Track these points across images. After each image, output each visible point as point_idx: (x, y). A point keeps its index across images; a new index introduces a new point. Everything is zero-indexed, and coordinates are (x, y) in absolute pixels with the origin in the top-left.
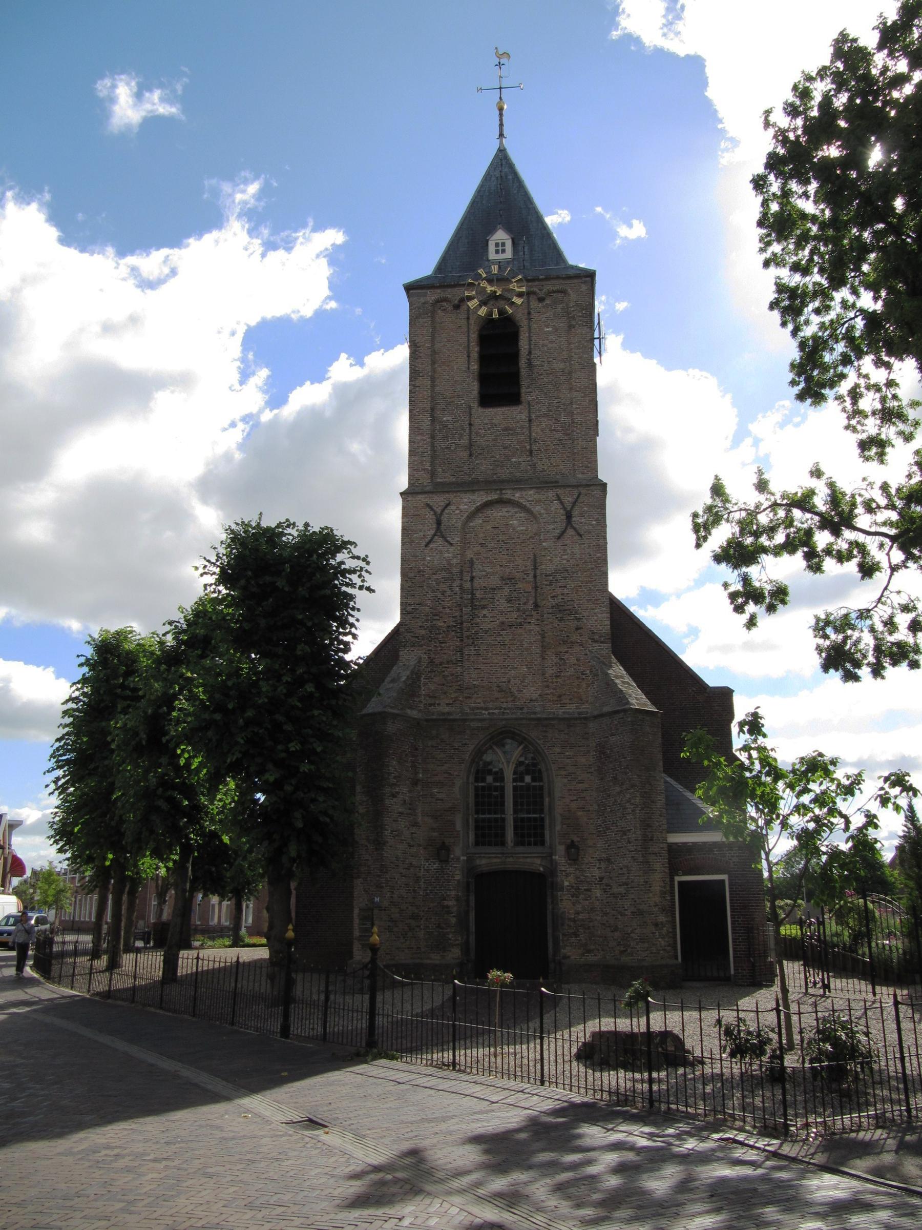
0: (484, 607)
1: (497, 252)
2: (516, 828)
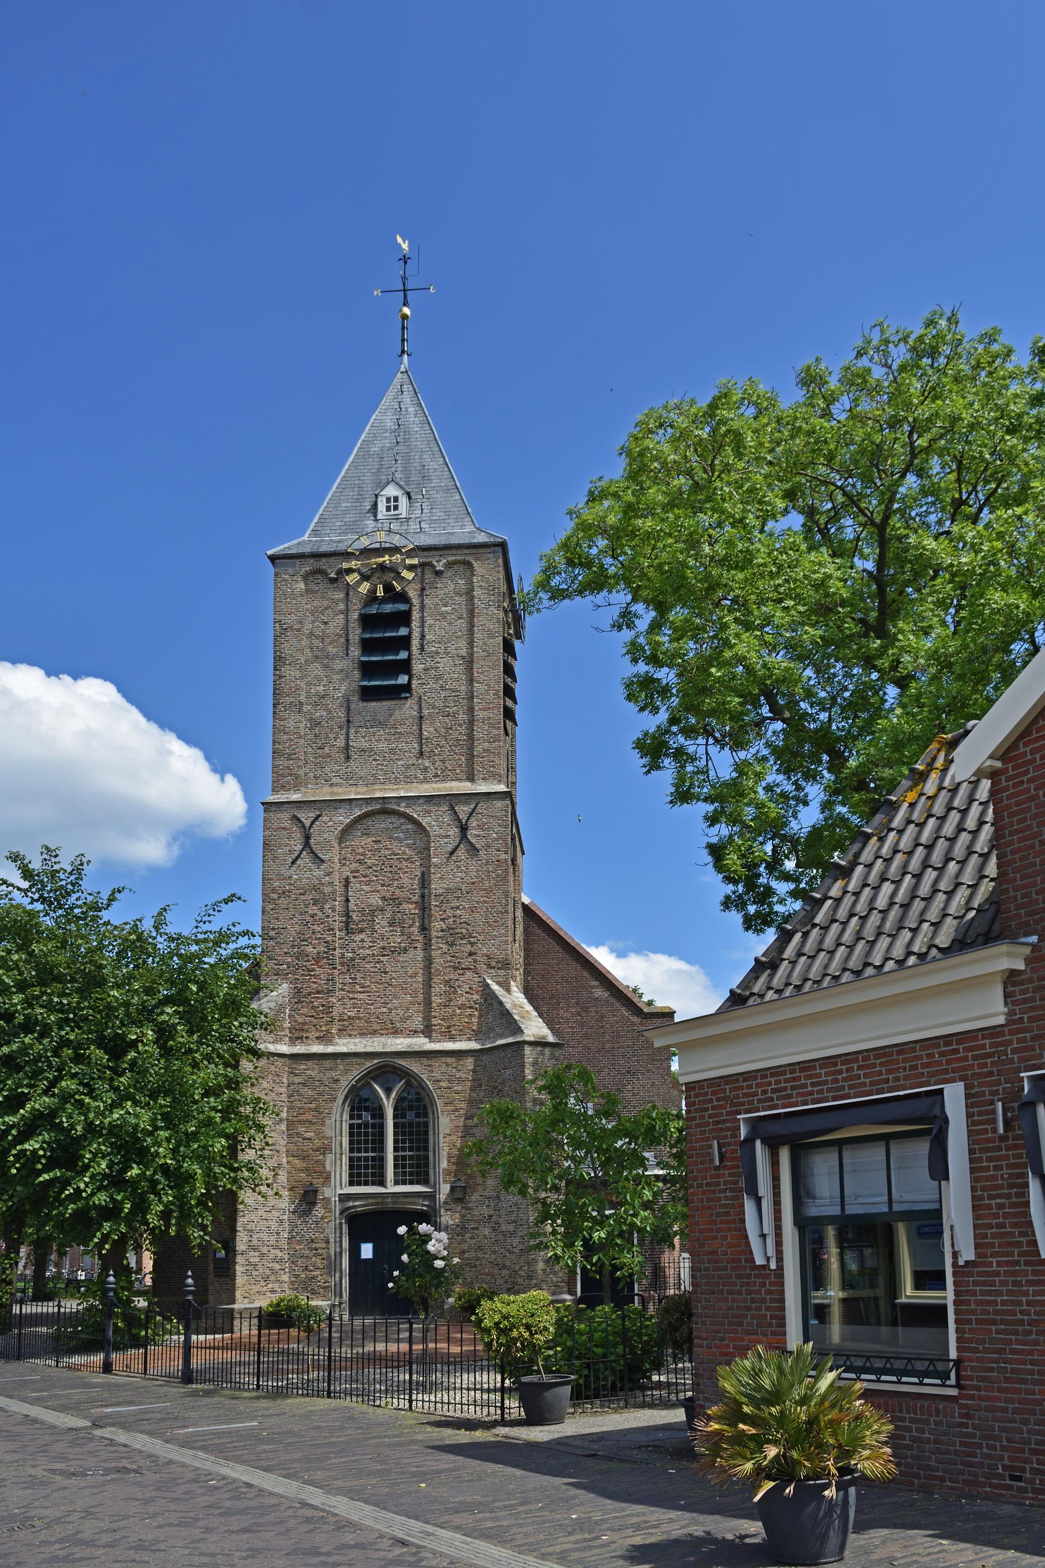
0: (361, 931)
1: (388, 509)
2: (396, 1166)
